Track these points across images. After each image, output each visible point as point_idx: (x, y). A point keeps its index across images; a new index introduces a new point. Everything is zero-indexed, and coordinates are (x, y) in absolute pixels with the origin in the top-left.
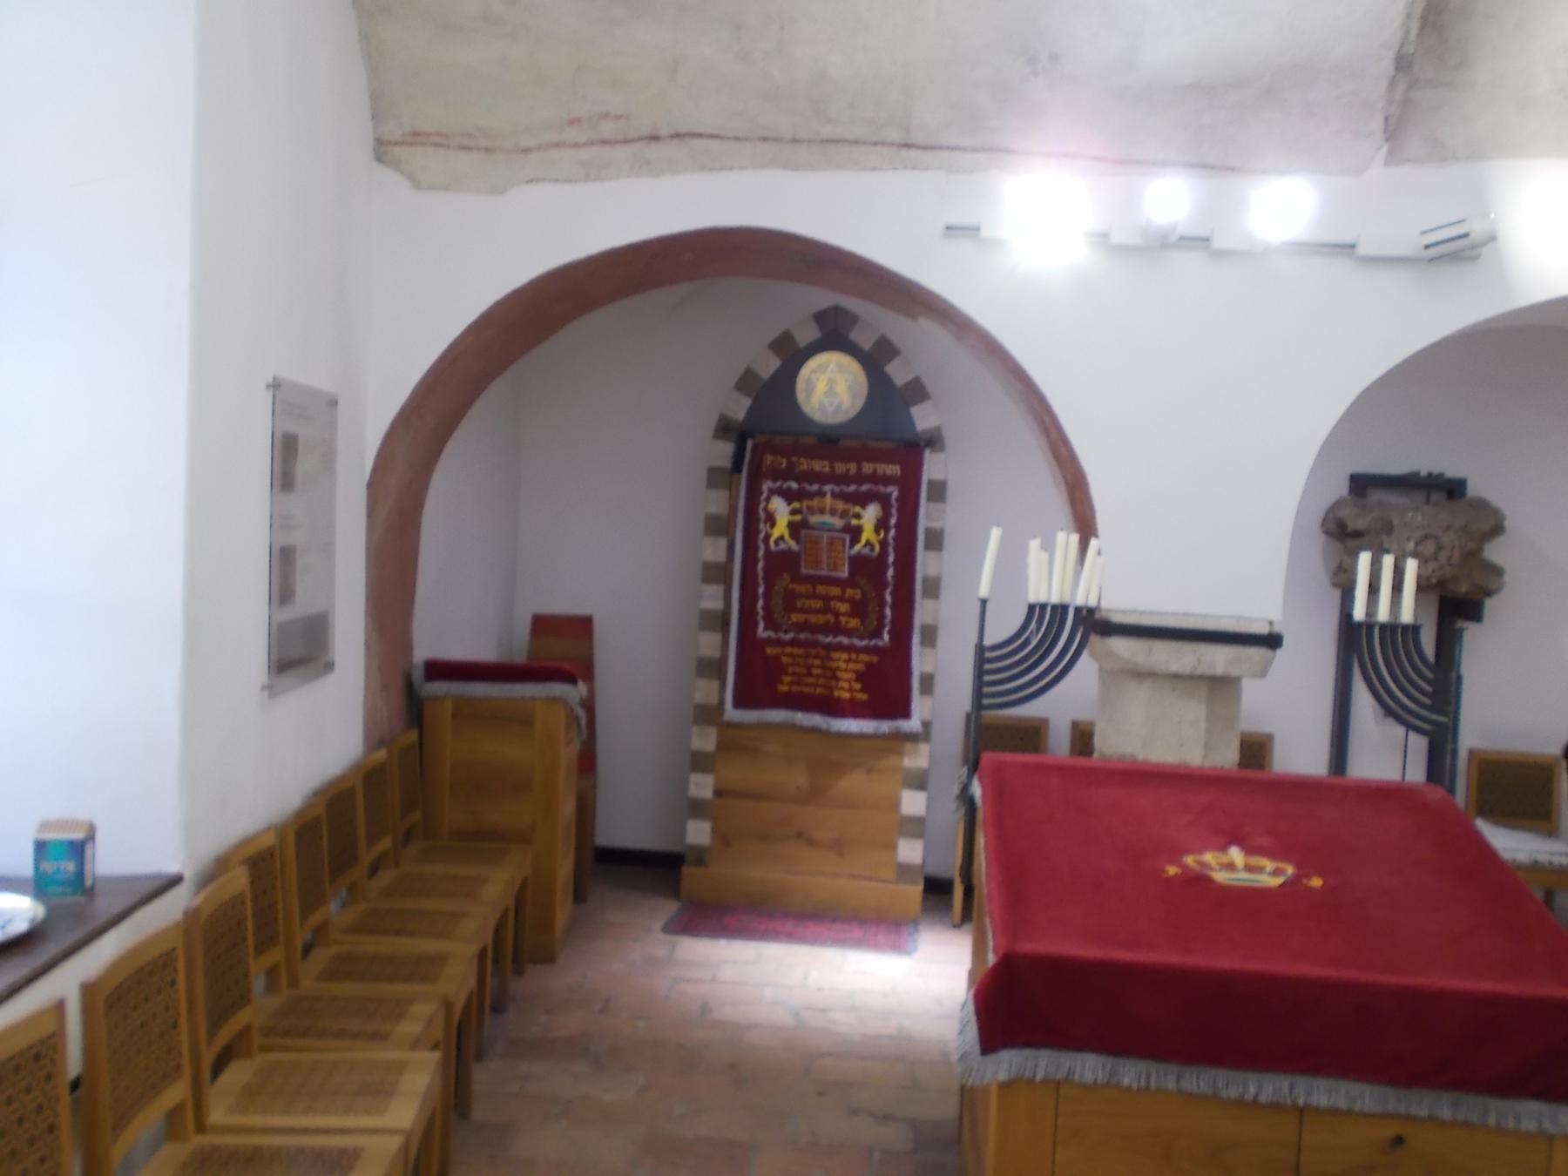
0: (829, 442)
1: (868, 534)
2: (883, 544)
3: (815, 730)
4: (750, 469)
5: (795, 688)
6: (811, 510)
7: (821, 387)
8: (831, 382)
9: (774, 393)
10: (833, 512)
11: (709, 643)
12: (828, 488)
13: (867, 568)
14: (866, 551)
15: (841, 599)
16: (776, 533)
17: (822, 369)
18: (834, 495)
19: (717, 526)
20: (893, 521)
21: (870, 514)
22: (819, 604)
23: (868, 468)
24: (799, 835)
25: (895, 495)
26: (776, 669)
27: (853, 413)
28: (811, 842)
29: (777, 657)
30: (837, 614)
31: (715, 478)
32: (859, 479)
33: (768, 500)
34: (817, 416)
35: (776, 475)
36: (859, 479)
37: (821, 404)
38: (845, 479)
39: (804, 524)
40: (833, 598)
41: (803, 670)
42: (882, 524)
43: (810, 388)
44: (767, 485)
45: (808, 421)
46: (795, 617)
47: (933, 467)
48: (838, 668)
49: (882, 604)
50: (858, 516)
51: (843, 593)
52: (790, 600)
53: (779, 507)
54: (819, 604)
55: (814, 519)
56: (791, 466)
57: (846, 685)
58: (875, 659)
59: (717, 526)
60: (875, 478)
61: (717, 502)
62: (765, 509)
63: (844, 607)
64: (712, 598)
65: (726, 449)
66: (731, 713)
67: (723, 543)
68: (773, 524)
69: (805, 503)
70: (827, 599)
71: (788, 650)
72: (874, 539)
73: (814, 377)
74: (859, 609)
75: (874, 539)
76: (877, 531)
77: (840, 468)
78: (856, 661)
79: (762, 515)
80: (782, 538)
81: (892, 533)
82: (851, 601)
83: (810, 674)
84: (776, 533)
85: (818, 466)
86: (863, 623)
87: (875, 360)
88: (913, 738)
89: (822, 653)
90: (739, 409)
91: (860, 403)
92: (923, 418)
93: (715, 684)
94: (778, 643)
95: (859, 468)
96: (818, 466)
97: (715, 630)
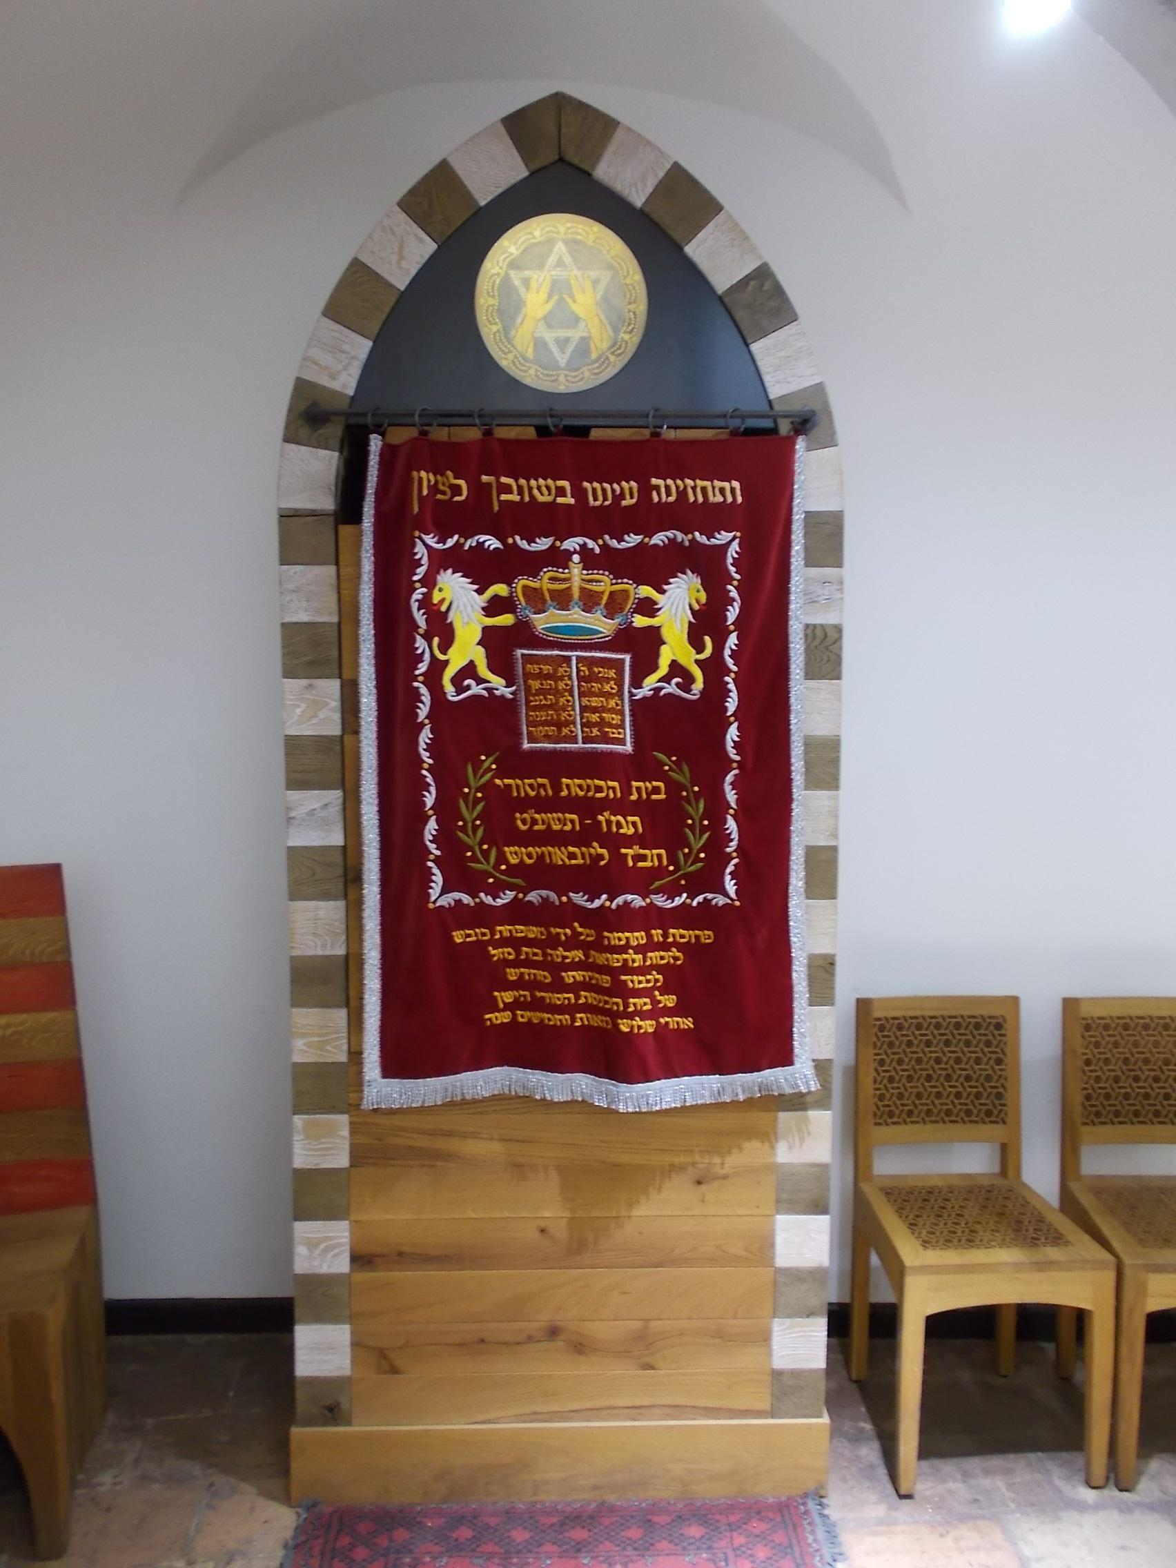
0: (563, 436)
1: (676, 647)
2: (713, 668)
3: (582, 1106)
4: (379, 515)
5: (523, 1016)
6: (536, 599)
7: (536, 303)
8: (559, 289)
9: (423, 320)
10: (589, 601)
11: (316, 927)
12: (572, 544)
13: (677, 728)
14: (671, 689)
15: (621, 806)
16: (456, 659)
17: (534, 256)
18: (589, 560)
19: (311, 652)
20: (732, 614)
21: (679, 599)
22: (570, 821)
23: (665, 489)
24: (553, 1332)
25: (734, 550)
26: (477, 974)
27: (616, 365)
28: (580, 1347)
29: (480, 947)
30: (614, 841)
31: (298, 536)
32: (647, 516)
33: (429, 581)
34: (531, 377)
35: (448, 519)
36: (647, 516)
37: (540, 344)
38: (612, 520)
39: (523, 634)
40: (605, 805)
41: (544, 976)
42: (705, 623)
43: (510, 308)
44: (425, 545)
45: (515, 385)
46: (514, 855)
47: (815, 481)
48: (626, 969)
49: (717, 810)
50: (647, 607)
51: (626, 790)
52: (500, 819)
53: (459, 596)
54: (570, 821)
55: (542, 622)
56: (481, 493)
57: (644, 1003)
58: (707, 936)
59: (311, 652)
60: (682, 514)
61: (309, 594)
62: (425, 603)
63: (629, 825)
64: (315, 821)
65: (320, 466)
66: (380, 1089)
67: (331, 688)
68: (448, 639)
69: (521, 582)
70: (588, 807)
71: (504, 930)
72: (689, 658)
73: (516, 278)
74: (664, 825)
75: (689, 658)
76: (695, 641)
77: (598, 493)
78: (665, 946)
79: (420, 618)
80: (469, 670)
81: (733, 640)
82: (642, 807)
83: (558, 986)
84: (456, 659)
85: (543, 490)
86: (673, 860)
87: (659, 230)
88: (797, 1102)
89: (587, 934)
90: (343, 365)
91: (631, 340)
92: (783, 367)
93: (340, 1016)
94: (482, 916)
95: (645, 490)
96: (543, 490)
97: (326, 896)
